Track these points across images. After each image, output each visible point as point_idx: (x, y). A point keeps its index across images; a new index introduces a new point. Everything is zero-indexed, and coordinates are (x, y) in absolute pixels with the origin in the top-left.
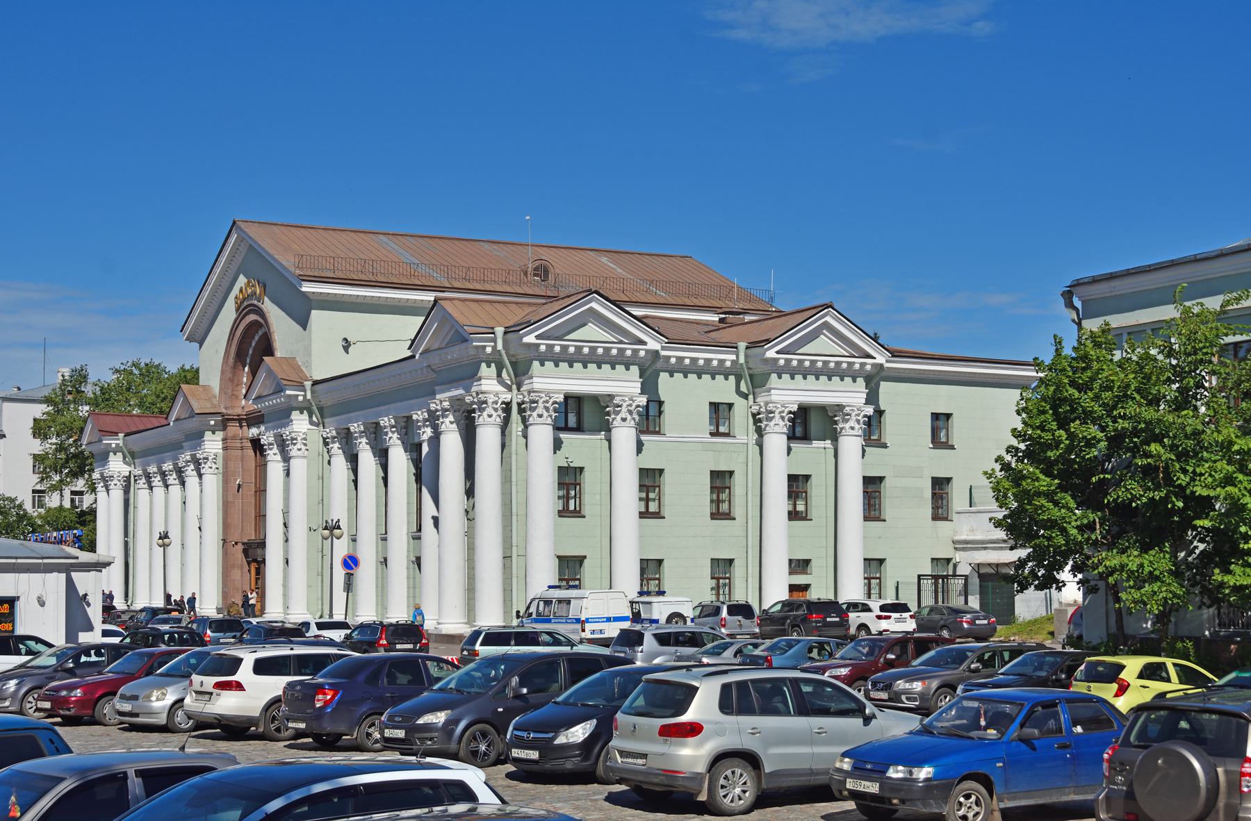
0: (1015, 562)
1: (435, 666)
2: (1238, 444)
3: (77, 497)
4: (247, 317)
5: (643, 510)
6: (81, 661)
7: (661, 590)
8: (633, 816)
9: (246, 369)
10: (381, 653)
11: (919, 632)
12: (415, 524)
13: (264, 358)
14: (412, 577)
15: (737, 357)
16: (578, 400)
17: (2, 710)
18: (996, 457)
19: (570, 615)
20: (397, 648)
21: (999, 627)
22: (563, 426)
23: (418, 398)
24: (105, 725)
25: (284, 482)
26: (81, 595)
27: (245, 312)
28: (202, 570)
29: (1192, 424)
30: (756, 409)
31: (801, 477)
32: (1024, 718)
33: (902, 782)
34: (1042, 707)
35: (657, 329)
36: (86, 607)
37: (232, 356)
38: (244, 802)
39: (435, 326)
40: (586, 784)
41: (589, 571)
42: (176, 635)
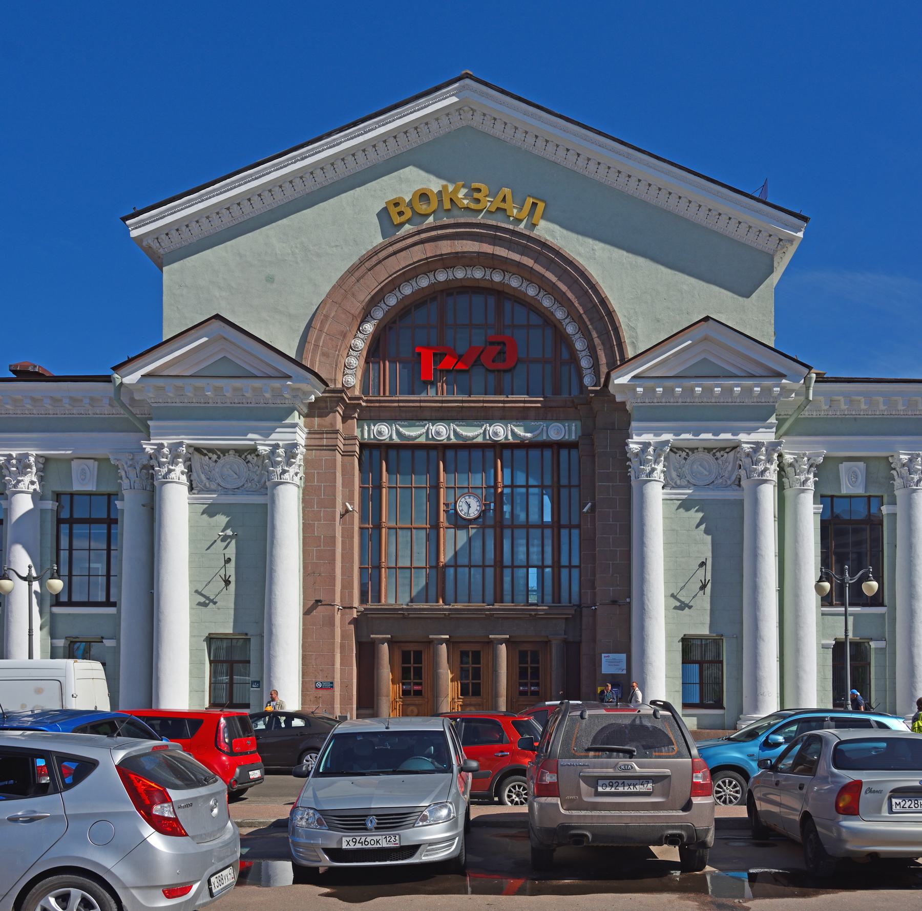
0: (321, 605)
1: (477, 510)
2: (346, 312)
3: (597, 484)
4: (473, 207)
5: (113, 526)
6: (320, 872)
7: (112, 516)
8: (370, 798)
9: (369, 327)
10: (187, 440)
11: (481, 769)
12: (425, 555)
13: (504, 644)
14: (548, 561)
15: (501, 642)
16: (211, 640)
17: (912, 779)
18: (682, 636)
19: (424, 526)
20: (251, 777)
21: (557, 849)
22: (104, 599)
23: (84, 431)
24: (51, 397)
25: (190, 614)
26: (228, 519)
27: (440, 232)
28: (540, 505)
29: (676, 751)
30: (265, 451)
31: (62, 654)
32: (149, 216)
33: (250, 837)
34: (296, 867)
35: (795, 357)
36: (696, 509)
37: (49, 545)
38: (898, 726)
39: (499, 234)
40: (101, 877)
41: (418, 700)
42: (170, 722)
